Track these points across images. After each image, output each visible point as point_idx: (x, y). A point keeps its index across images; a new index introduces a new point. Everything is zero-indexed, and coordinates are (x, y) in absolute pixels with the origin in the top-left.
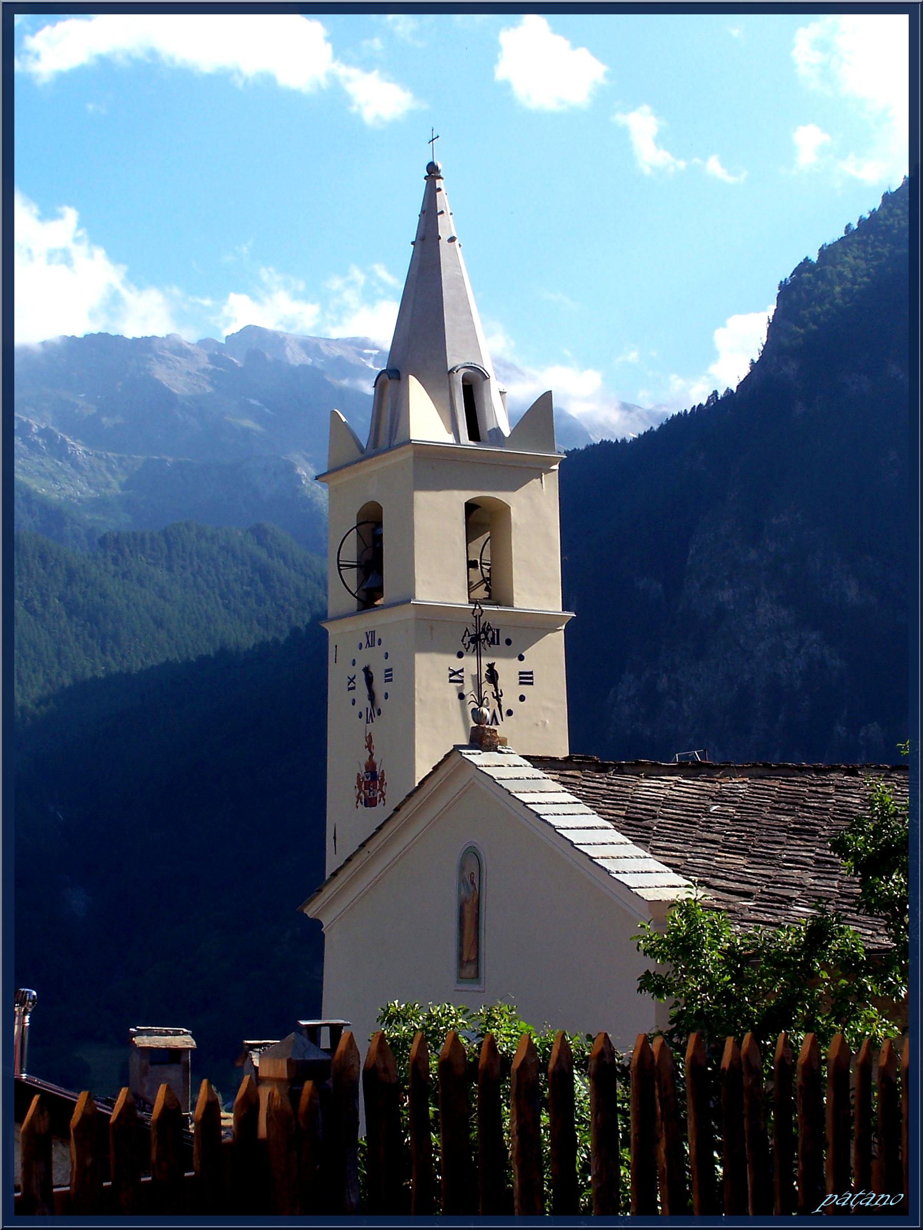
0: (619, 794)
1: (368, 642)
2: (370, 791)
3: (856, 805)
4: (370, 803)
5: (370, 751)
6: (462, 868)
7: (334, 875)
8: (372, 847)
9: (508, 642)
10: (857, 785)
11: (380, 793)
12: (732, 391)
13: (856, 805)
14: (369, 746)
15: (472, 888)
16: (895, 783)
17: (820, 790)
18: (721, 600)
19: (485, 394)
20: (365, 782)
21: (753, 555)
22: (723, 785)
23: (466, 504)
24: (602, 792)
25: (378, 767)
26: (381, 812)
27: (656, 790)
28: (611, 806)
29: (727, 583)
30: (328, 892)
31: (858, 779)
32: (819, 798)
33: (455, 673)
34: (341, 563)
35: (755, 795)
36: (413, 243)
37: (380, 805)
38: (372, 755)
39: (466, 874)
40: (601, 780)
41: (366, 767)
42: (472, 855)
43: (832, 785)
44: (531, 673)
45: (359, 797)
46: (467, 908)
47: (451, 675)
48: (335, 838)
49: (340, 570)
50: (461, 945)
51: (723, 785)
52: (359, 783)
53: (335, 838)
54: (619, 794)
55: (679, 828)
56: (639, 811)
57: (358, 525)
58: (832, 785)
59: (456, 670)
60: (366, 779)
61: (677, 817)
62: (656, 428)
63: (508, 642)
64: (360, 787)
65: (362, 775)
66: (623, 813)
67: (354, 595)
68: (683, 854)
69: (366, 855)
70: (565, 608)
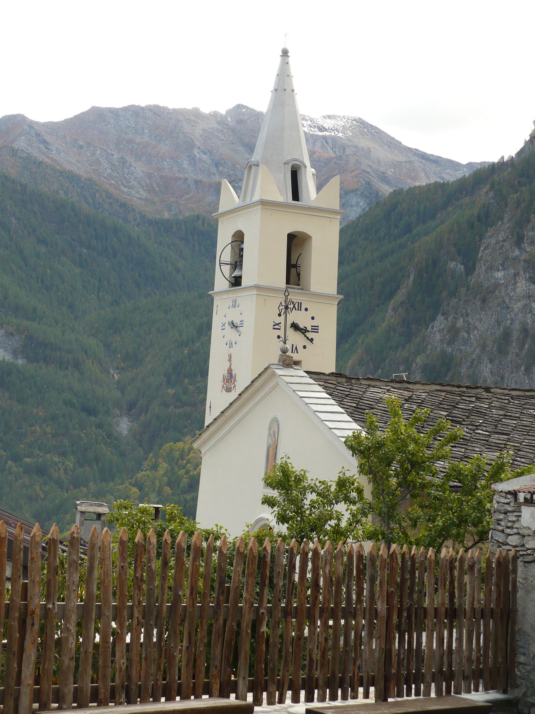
0: (355, 395)
1: (233, 305)
2: (229, 384)
3: (486, 409)
4: (229, 390)
5: (230, 362)
6: (270, 428)
7: (208, 427)
8: (227, 414)
9: (306, 310)
10: (489, 397)
11: (233, 385)
12: (512, 157)
13: (486, 409)
14: (230, 360)
15: (274, 439)
16: (510, 398)
17: (467, 399)
18: (497, 277)
19: (303, 176)
20: (227, 379)
21: (517, 253)
22: (414, 393)
23: (288, 235)
24: (346, 393)
25: (233, 371)
26: (233, 395)
27: (376, 394)
28: (349, 401)
29: (501, 267)
30: (205, 436)
31: (490, 394)
32: (466, 403)
33: (276, 325)
34: (221, 262)
35: (431, 400)
36: (272, 92)
37: (233, 392)
38: (231, 364)
39: (272, 431)
40: (347, 387)
41: (228, 370)
42: (275, 421)
43: (474, 396)
44: (318, 327)
45: (223, 387)
46: (271, 449)
47: (274, 326)
48: (210, 407)
49: (220, 266)
50: (267, 468)
51: (414, 393)
52: (224, 379)
53: (210, 407)
54: (355, 395)
55: (384, 415)
56: (364, 405)
57: (232, 242)
58: (474, 396)
59: (277, 323)
60: (227, 377)
61: (384, 409)
62: (472, 173)
63: (306, 310)
64: (224, 381)
65: (226, 375)
66: (355, 405)
67: (227, 279)
68: (383, 429)
69: (224, 417)
70: (338, 293)
